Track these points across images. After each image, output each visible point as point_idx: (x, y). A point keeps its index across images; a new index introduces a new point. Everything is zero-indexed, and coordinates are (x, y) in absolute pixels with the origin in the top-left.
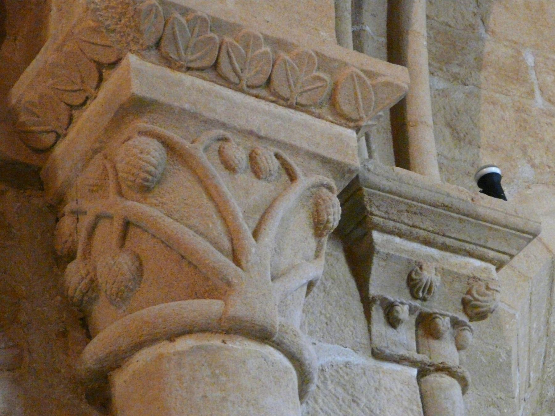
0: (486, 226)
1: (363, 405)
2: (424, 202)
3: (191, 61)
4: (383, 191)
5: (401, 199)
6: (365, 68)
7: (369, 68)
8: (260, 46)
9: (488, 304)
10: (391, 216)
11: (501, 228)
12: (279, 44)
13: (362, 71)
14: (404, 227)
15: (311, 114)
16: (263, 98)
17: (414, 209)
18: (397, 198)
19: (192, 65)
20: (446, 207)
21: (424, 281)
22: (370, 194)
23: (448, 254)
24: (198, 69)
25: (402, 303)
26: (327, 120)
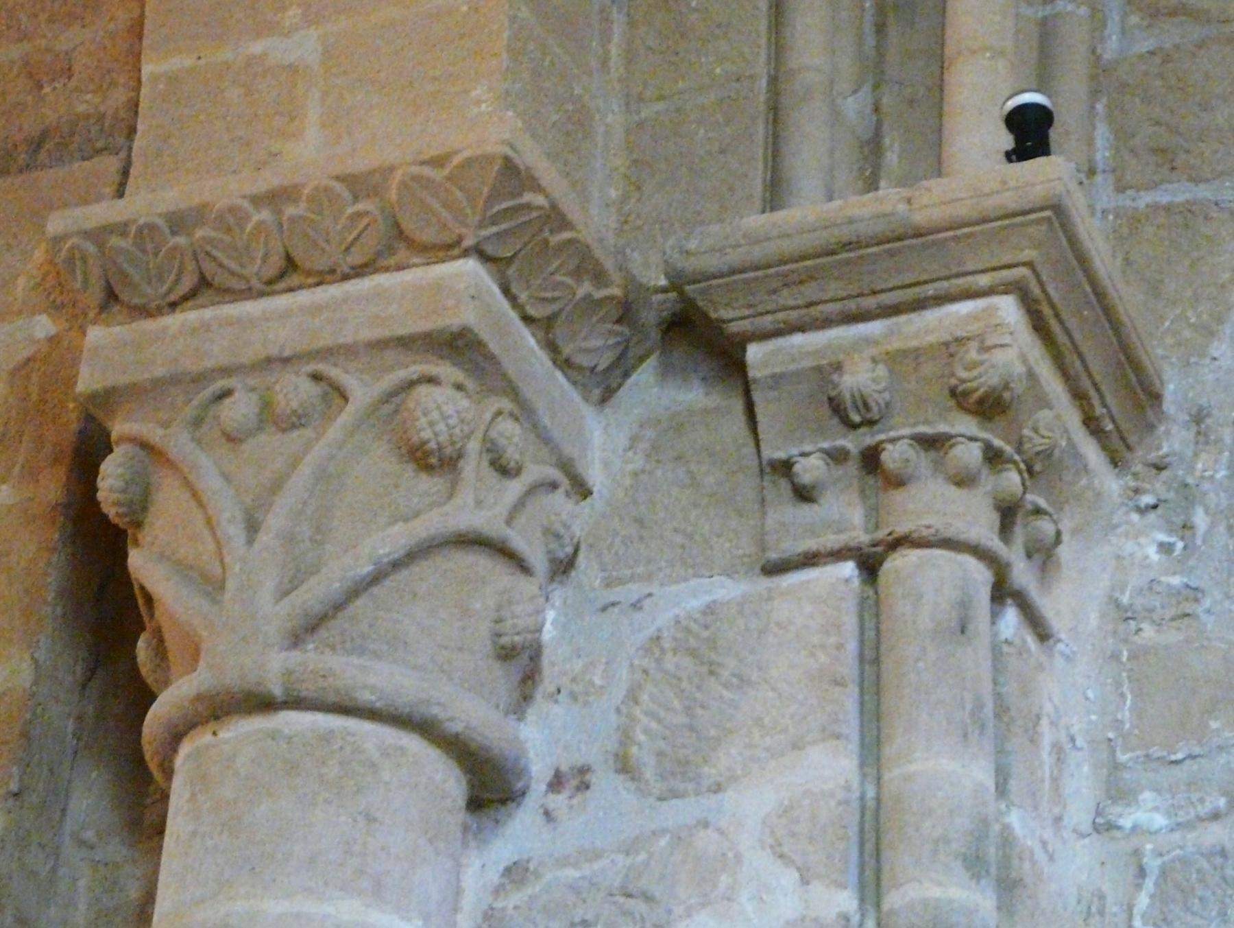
0: (946, 239)
1: (726, 673)
2: (804, 258)
3: (169, 291)
4: (722, 276)
5: (760, 273)
6: (426, 157)
7: (434, 152)
8: (247, 217)
9: (982, 380)
10: (760, 309)
11: (977, 228)
12: (275, 198)
13: (423, 163)
14: (794, 315)
15: (387, 269)
16: (300, 287)
17: (795, 277)
18: (752, 274)
19: (172, 297)
20: (847, 246)
21: (848, 396)
22: (703, 292)
23: (902, 318)
24: (185, 298)
25: (804, 455)
26: (416, 265)
